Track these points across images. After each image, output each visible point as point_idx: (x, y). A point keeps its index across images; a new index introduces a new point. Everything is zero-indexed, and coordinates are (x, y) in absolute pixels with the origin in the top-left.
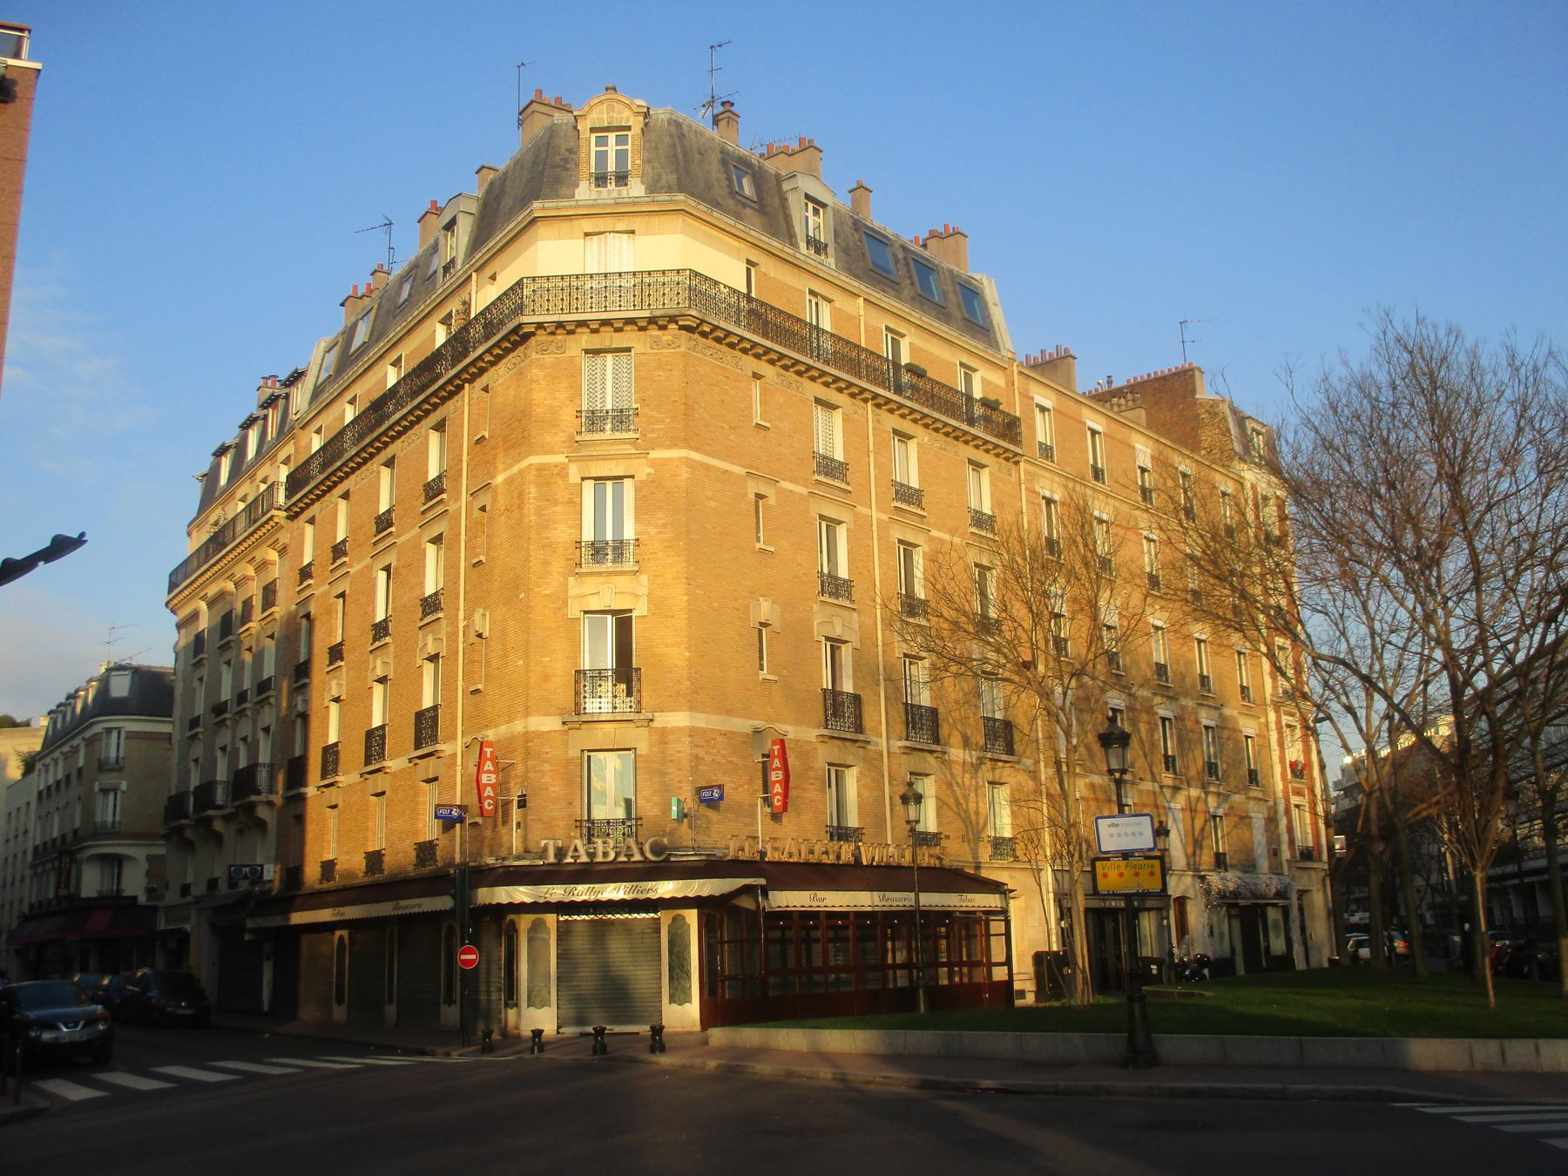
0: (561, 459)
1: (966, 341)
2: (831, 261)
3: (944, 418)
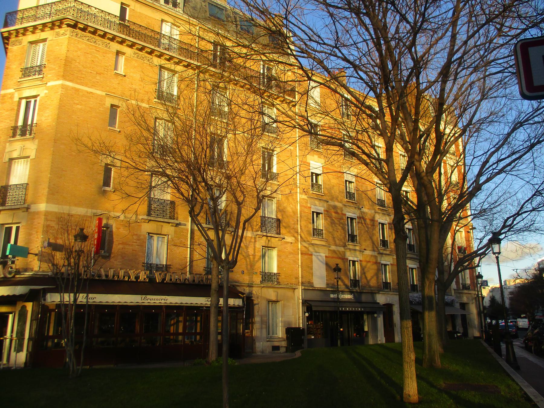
0: (11, 91)
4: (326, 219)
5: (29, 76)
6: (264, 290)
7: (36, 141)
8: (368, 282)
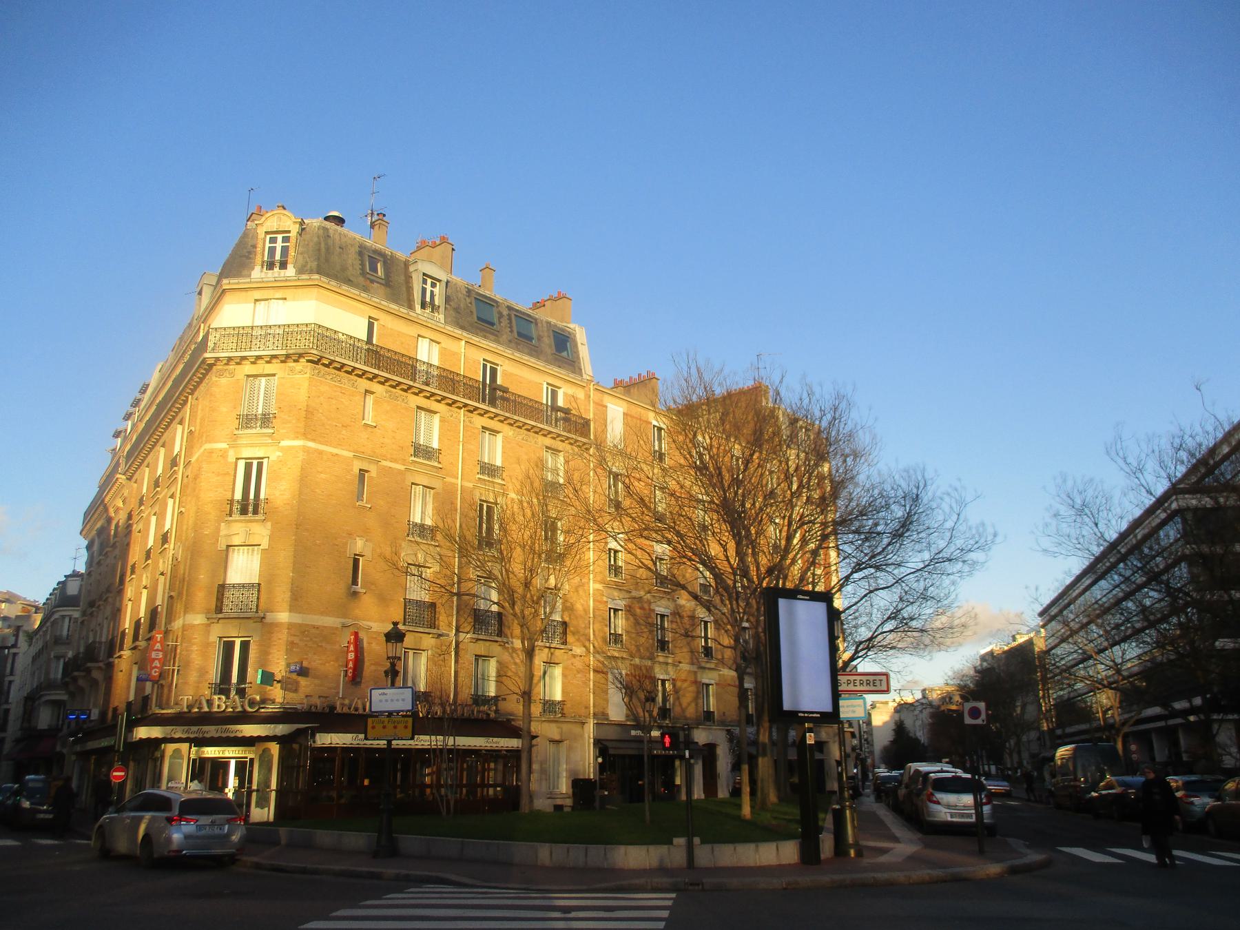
0: (223, 446)
1: (555, 370)
2: (442, 317)
3: (522, 419)
4: (627, 619)
5: (251, 427)
6: (546, 725)
7: (269, 524)
8: (683, 710)
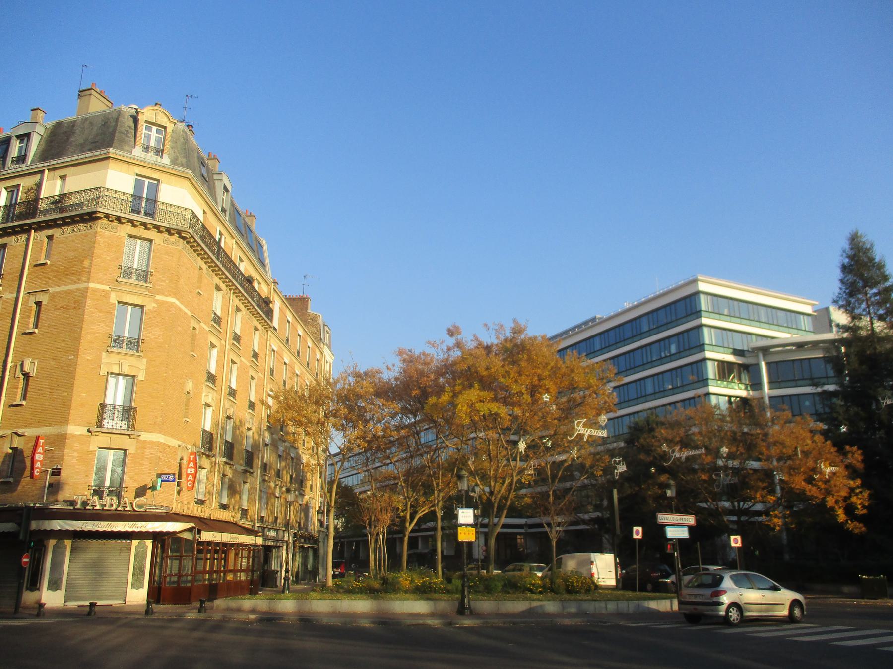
0: (106, 288)
